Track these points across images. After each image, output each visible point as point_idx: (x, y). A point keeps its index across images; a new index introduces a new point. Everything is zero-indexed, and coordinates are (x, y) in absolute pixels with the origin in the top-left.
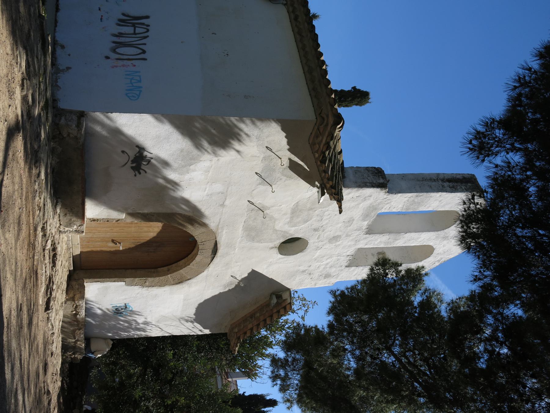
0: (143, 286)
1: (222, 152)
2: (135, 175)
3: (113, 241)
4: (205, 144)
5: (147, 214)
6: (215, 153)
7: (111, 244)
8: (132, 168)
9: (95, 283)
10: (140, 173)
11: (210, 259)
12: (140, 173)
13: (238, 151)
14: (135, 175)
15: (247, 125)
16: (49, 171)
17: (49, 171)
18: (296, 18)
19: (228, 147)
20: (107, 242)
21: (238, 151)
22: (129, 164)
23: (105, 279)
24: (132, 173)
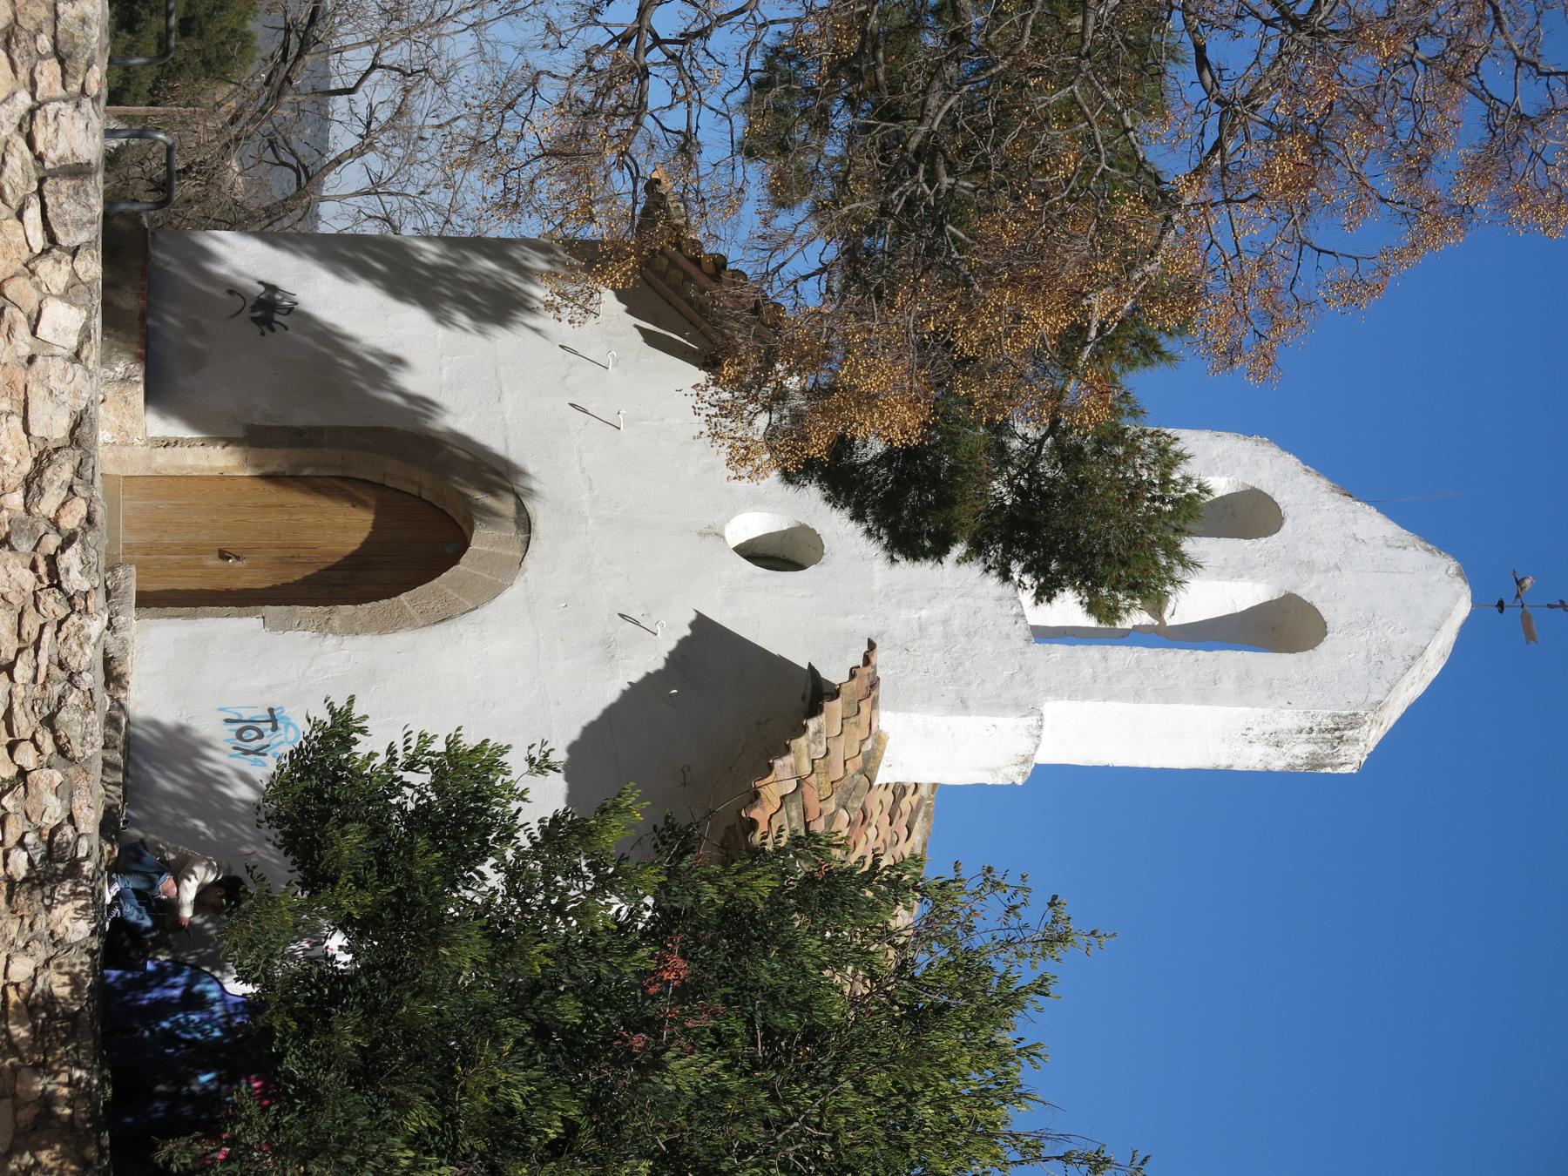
0: (323, 629)
1: (498, 332)
2: (263, 334)
3: (223, 555)
4: (462, 319)
5: (310, 429)
6: (481, 332)
7: (213, 562)
8: (254, 320)
9: (165, 621)
10: (273, 330)
11: (519, 546)
12: (273, 330)
13: (536, 330)
14: (263, 334)
15: (536, 284)
16: (348, 254)
17: (348, 254)
18: (231, 292)
19: (512, 321)
20: (206, 552)
21: (536, 330)
22: (247, 313)
23: (200, 609)
24: (255, 329)
